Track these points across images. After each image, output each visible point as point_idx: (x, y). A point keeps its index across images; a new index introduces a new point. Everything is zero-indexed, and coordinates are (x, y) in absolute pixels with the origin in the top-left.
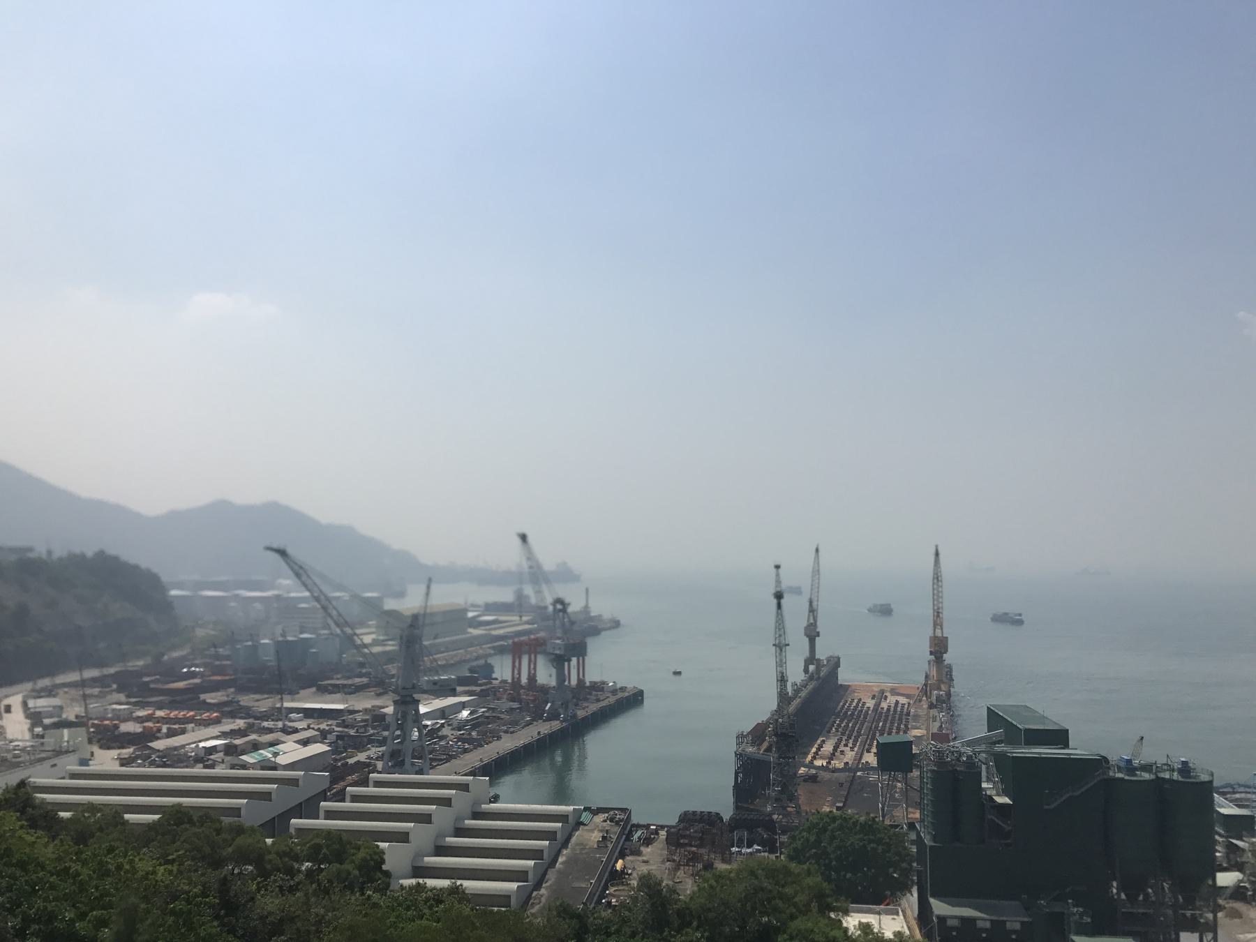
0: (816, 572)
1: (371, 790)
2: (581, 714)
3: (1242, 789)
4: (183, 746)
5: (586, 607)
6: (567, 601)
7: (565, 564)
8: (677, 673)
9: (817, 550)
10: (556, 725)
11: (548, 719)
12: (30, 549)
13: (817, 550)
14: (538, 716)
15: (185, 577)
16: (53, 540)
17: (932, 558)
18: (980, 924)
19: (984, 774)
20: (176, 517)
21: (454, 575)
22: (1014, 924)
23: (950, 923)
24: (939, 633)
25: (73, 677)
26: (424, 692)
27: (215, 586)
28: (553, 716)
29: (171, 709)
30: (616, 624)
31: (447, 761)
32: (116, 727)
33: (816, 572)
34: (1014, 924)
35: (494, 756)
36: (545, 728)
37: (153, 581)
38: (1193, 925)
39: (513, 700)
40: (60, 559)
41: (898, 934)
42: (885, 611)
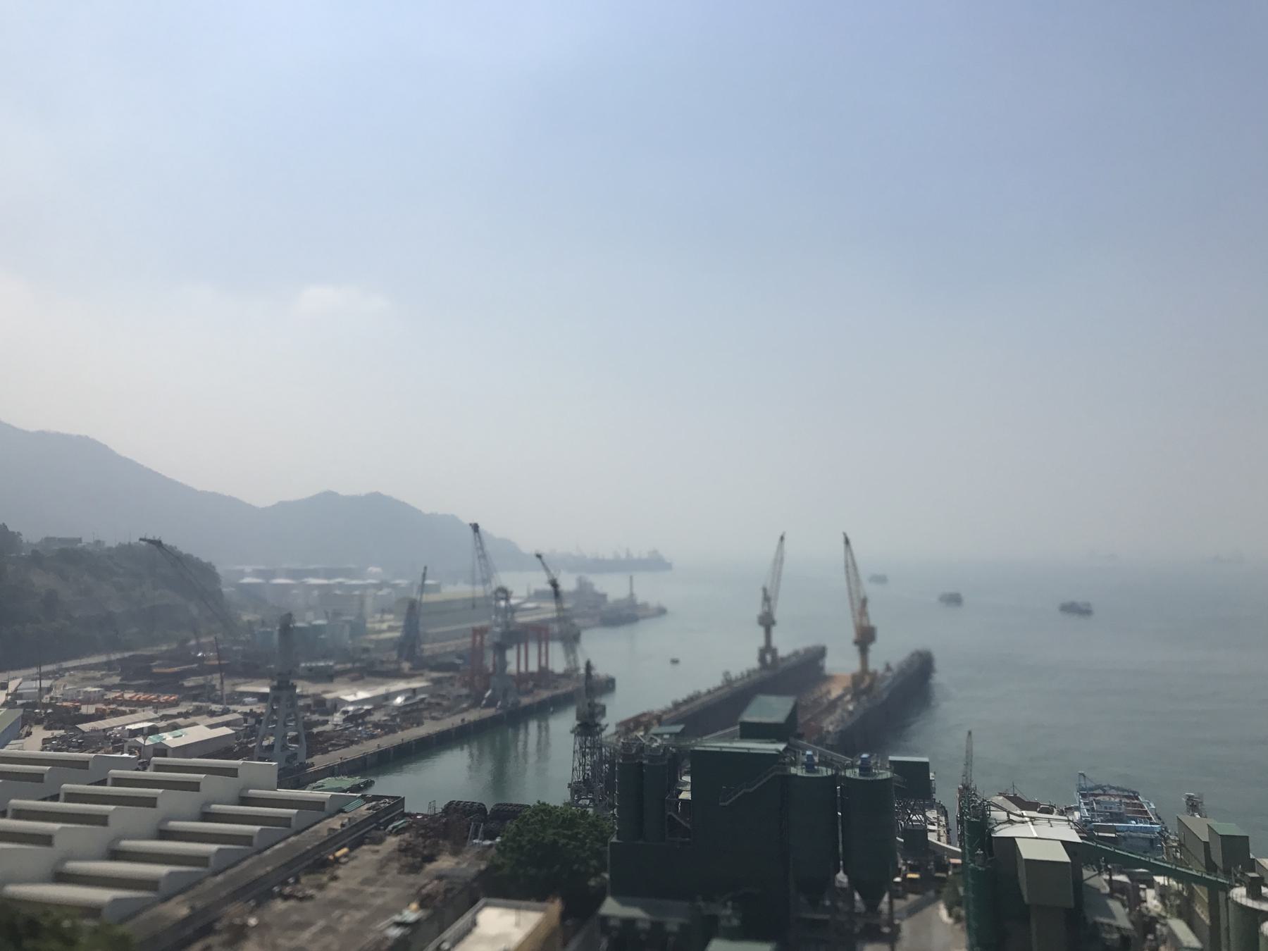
0: (779, 560)
1: (149, 774)
2: (525, 701)
3: (1113, 792)
4: (112, 728)
5: (632, 594)
6: (510, 589)
7: (655, 552)
8: (675, 662)
9: (782, 538)
10: (490, 712)
11: (487, 706)
12: (80, 540)
13: (782, 538)
14: (476, 704)
15: (239, 569)
16: (112, 528)
17: (842, 545)
18: (640, 925)
19: (779, 773)
20: (284, 507)
21: (601, 566)
22: (673, 924)
23: (612, 923)
24: (865, 623)
25: (102, 658)
26: (301, 678)
27: (315, 573)
28: (491, 703)
29: (145, 692)
30: (662, 611)
31: (346, 746)
32: (78, 709)
33: (779, 560)
34: (673, 924)
35: (399, 741)
36: (473, 716)
37: (207, 571)
38: (873, 935)
39: (464, 686)
40: (110, 549)
41: (682, 926)
42: (954, 600)
